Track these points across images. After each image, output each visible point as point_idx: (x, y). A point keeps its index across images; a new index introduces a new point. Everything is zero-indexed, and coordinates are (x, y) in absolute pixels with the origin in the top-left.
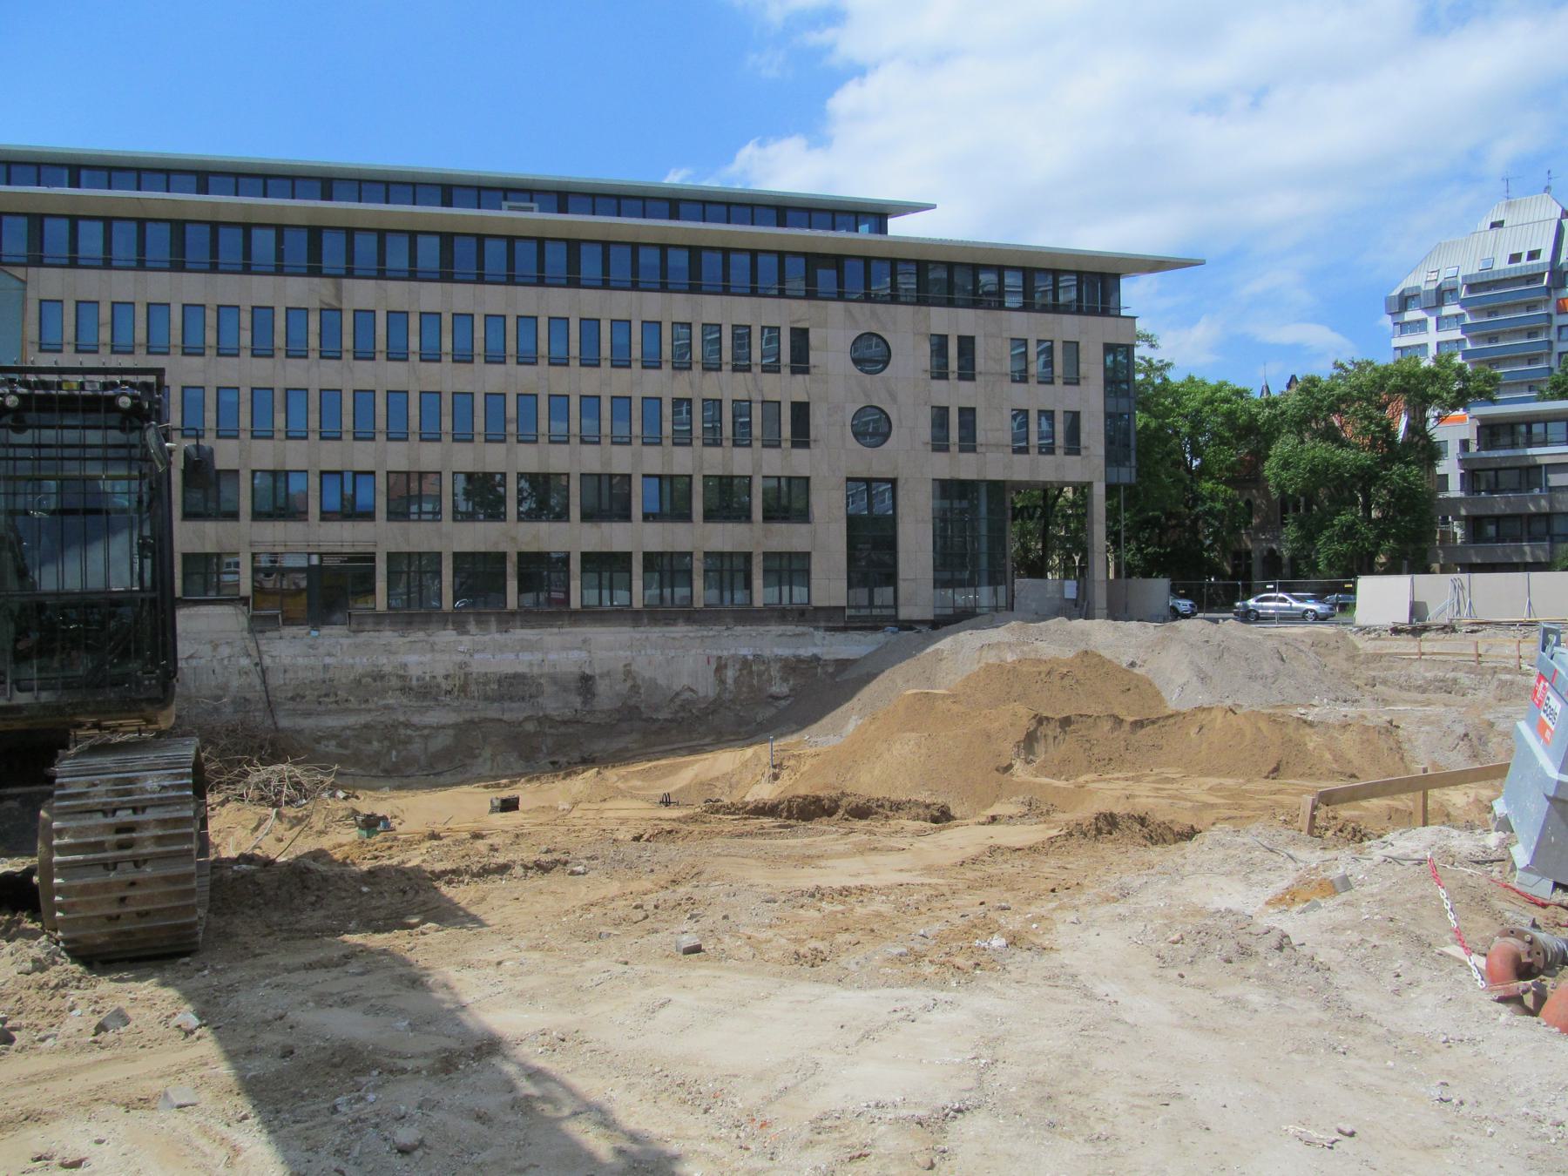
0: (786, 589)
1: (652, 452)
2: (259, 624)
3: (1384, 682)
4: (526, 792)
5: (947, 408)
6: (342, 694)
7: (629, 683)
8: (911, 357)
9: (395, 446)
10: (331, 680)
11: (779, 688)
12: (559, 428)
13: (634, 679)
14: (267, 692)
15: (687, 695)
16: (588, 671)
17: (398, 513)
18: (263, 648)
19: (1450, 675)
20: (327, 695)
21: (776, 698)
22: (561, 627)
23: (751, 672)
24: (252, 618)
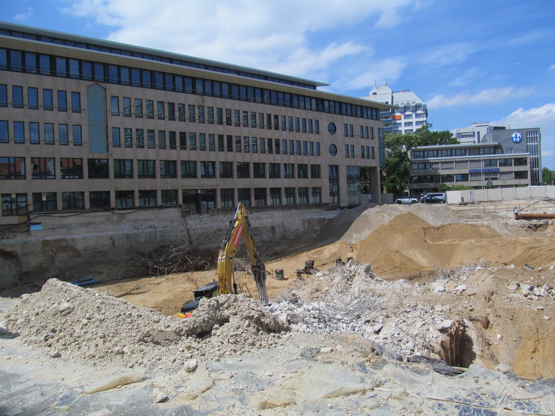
0: (226, 202)
1: (255, 155)
2: (185, 214)
3: (463, 217)
4: (33, 294)
5: (175, 132)
6: (211, 237)
7: (283, 229)
8: (340, 130)
9: (139, 150)
10: (208, 232)
11: (317, 228)
12: (35, 137)
13: (284, 227)
14: (189, 237)
15: (297, 231)
16: (274, 226)
17: (119, 175)
18: (187, 222)
19: (479, 214)
20: (206, 237)
21: (316, 231)
22: (265, 212)
23: (310, 223)
24: (182, 212)
